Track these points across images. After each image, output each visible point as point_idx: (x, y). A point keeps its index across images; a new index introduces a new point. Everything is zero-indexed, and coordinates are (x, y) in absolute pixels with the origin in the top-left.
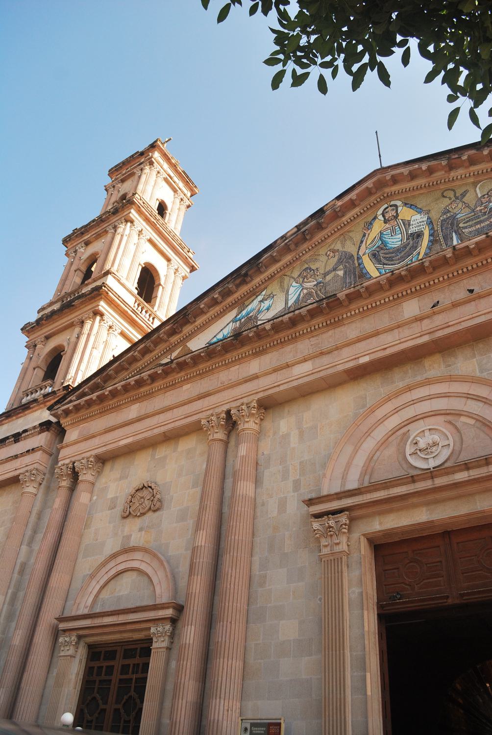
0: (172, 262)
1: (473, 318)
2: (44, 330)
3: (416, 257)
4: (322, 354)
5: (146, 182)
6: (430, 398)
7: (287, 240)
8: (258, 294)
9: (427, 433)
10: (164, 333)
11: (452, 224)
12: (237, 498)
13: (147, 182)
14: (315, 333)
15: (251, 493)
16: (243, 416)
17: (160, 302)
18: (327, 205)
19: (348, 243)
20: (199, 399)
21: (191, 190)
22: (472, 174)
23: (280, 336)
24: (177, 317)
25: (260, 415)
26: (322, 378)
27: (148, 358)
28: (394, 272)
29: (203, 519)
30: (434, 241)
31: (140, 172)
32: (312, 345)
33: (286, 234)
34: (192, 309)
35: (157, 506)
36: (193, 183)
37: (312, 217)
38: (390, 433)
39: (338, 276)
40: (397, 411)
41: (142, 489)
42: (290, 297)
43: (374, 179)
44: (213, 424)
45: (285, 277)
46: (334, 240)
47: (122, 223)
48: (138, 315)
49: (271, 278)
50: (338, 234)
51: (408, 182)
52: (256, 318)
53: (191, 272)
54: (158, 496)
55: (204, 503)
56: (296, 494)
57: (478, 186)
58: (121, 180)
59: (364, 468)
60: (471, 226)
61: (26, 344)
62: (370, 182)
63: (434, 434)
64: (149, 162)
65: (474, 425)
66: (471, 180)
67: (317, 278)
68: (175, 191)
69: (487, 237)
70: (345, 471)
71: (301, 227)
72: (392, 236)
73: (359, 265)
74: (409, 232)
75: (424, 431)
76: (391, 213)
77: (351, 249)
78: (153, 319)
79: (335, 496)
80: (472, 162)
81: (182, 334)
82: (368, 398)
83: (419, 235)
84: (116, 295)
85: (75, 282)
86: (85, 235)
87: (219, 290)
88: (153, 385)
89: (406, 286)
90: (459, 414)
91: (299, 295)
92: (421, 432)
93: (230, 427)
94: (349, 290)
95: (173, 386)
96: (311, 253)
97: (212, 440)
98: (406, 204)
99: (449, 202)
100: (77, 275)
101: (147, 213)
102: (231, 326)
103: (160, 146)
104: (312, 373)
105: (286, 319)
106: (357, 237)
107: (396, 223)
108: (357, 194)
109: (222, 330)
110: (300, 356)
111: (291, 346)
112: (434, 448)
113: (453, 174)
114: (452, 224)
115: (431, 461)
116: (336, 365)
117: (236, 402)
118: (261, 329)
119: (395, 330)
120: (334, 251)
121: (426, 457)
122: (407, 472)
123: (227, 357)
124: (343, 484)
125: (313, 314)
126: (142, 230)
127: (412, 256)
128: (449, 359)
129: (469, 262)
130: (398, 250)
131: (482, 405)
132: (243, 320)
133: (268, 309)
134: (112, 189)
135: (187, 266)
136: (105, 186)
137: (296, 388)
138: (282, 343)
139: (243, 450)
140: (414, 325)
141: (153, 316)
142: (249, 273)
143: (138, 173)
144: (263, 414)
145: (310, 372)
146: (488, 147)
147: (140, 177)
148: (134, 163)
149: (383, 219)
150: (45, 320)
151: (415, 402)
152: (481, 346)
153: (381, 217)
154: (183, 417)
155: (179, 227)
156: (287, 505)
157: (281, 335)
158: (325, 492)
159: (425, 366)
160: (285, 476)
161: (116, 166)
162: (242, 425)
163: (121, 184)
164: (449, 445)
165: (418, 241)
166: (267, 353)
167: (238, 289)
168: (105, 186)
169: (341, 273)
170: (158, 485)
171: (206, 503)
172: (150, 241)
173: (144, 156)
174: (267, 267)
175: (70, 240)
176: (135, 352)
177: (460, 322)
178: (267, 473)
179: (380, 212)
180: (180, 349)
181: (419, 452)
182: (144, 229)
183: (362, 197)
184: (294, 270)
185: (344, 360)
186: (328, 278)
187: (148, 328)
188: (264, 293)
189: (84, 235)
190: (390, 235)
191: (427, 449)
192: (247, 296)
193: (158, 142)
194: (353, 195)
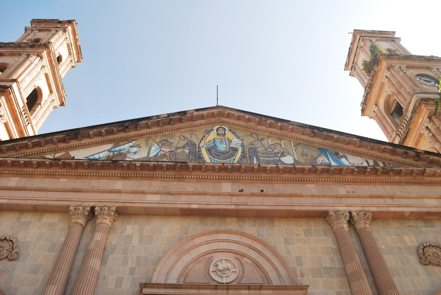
0: (53, 94)
1: (260, 205)
3: (233, 161)
4: (168, 193)
5: (57, 40)
6: (228, 241)
7: (160, 119)
8: (130, 141)
9: (224, 261)
10: (57, 138)
11: (254, 152)
12: (89, 269)
13: (58, 40)
14: (165, 180)
15: (98, 268)
16: (104, 214)
17: (36, 115)
18: (189, 111)
19: (194, 136)
20: (72, 191)
21: (79, 59)
22: (268, 131)
23: (143, 173)
24: (70, 132)
25: (115, 217)
26: (165, 208)
27: (36, 149)
28: (224, 164)
29: (57, 277)
30: (243, 156)
31: (55, 32)
32: (162, 186)
33: (160, 115)
34: (83, 132)
35: (14, 257)
36: (81, 55)
37: (179, 113)
38: (201, 255)
39: (185, 152)
40: (208, 243)
41: (3, 240)
43: (219, 110)
44: (79, 212)
45: (150, 139)
46: (186, 131)
47: (35, 55)
48: (22, 117)
49: (141, 136)
50: (188, 129)
51: (235, 120)
52: (125, 155)
53: (60, 105)
54: (17, 250)
55: (60, 265)
56: (131, 277)
57: (270, 138)
58: (39, 29)
59: (182, 272)
60: (264, 157)
62: (216, 110)
63: (227, 263)
64: (64, 30)
65: (251, 264)
66: (267, 134)
67: (172, 148)
68: (70, 54)
69: (277, 166)
70: (169, 270)
71: (170, 115)
73: (199, 151)
74: (231, 146)
75: (222, 259)
76: (221, 132)
77: (196, 141)
78: (28, 123)
79: (163, 286)
80: (271, 126)
81: (68, 144)
82: (190, 229)
83: (236, 150)
84: (15, 98)
86: (2, 49)
87: (107, 128)
88: (36, 170)
89: (228, 174)
90: (244, 256)
91: (158, 153)
92: (220, 260)
93: (90, 218)
94: (196, 163)
95: (53, 176)
96: (170, 132)
97: (76, 222)
98: (230, 131)
99: (254, 140)
102: (106, 154)
103: (74, 24)
104: (159, 203)
105: (152, 164)
106: (200, 136)
107: (223, 138)
108: (207, 113)
109: (98, 153)
110: (152, 189)
111: (148, 181)
112: (227, 272)
113: (259, 127)
114: (254, 152)
115: (224, 278)
116: (176, 203)
117: (100, 203)
118: (132, 164)
119: (216, 196)
121: (222, 275)
122: (209, 282)
123: (101, 172)
124: (166, 279)
125: (169, 168)
126: (45, 66)
128: (241, 223)
129: (264, 175)
130: (223, 153)
131: (257, 255)
132: (115, 153)
133: (135, 153)
134: (30, 31)
135: (60, 101)
136: (26, 27)
137: (146, 208)
138: (143, 178)
139: (98, 236)
140: (227, 197)
141: (29, 121)
142: (130, 127)
144: (116, 217)
145: (159, 202)
146: (281, 122)
147: (54, 35)
148: (52, 24)
149: (216, 132)
151: (219, 241)
152: (259, 221)
153: (215, 131)
154: (56, 199)
156: (123, 283)
157: (144, 172)
158: (154, 281)
159: (227, 222)
160: (125, 262)
162: (101, 219)
164: (236, 272)
165: (235, 153)
166: (130, 180)
168: (26, 27)
170: (18, 241)
171: (61, 266)
172: (46, 75)
173: (61, 24)
174: (142, 128)
177: (254, 205)
178: (111, 257)
180: (63, 153)
181: (217, 271)
182: (46, 66)
184: (157, 138)
185: (182, 202)
186: (179, 151)
187: (24, 128)
188: (134, 142)
191: (223, 271)
192: (122, 140)
193: (74, 22)
194: (205, 113)
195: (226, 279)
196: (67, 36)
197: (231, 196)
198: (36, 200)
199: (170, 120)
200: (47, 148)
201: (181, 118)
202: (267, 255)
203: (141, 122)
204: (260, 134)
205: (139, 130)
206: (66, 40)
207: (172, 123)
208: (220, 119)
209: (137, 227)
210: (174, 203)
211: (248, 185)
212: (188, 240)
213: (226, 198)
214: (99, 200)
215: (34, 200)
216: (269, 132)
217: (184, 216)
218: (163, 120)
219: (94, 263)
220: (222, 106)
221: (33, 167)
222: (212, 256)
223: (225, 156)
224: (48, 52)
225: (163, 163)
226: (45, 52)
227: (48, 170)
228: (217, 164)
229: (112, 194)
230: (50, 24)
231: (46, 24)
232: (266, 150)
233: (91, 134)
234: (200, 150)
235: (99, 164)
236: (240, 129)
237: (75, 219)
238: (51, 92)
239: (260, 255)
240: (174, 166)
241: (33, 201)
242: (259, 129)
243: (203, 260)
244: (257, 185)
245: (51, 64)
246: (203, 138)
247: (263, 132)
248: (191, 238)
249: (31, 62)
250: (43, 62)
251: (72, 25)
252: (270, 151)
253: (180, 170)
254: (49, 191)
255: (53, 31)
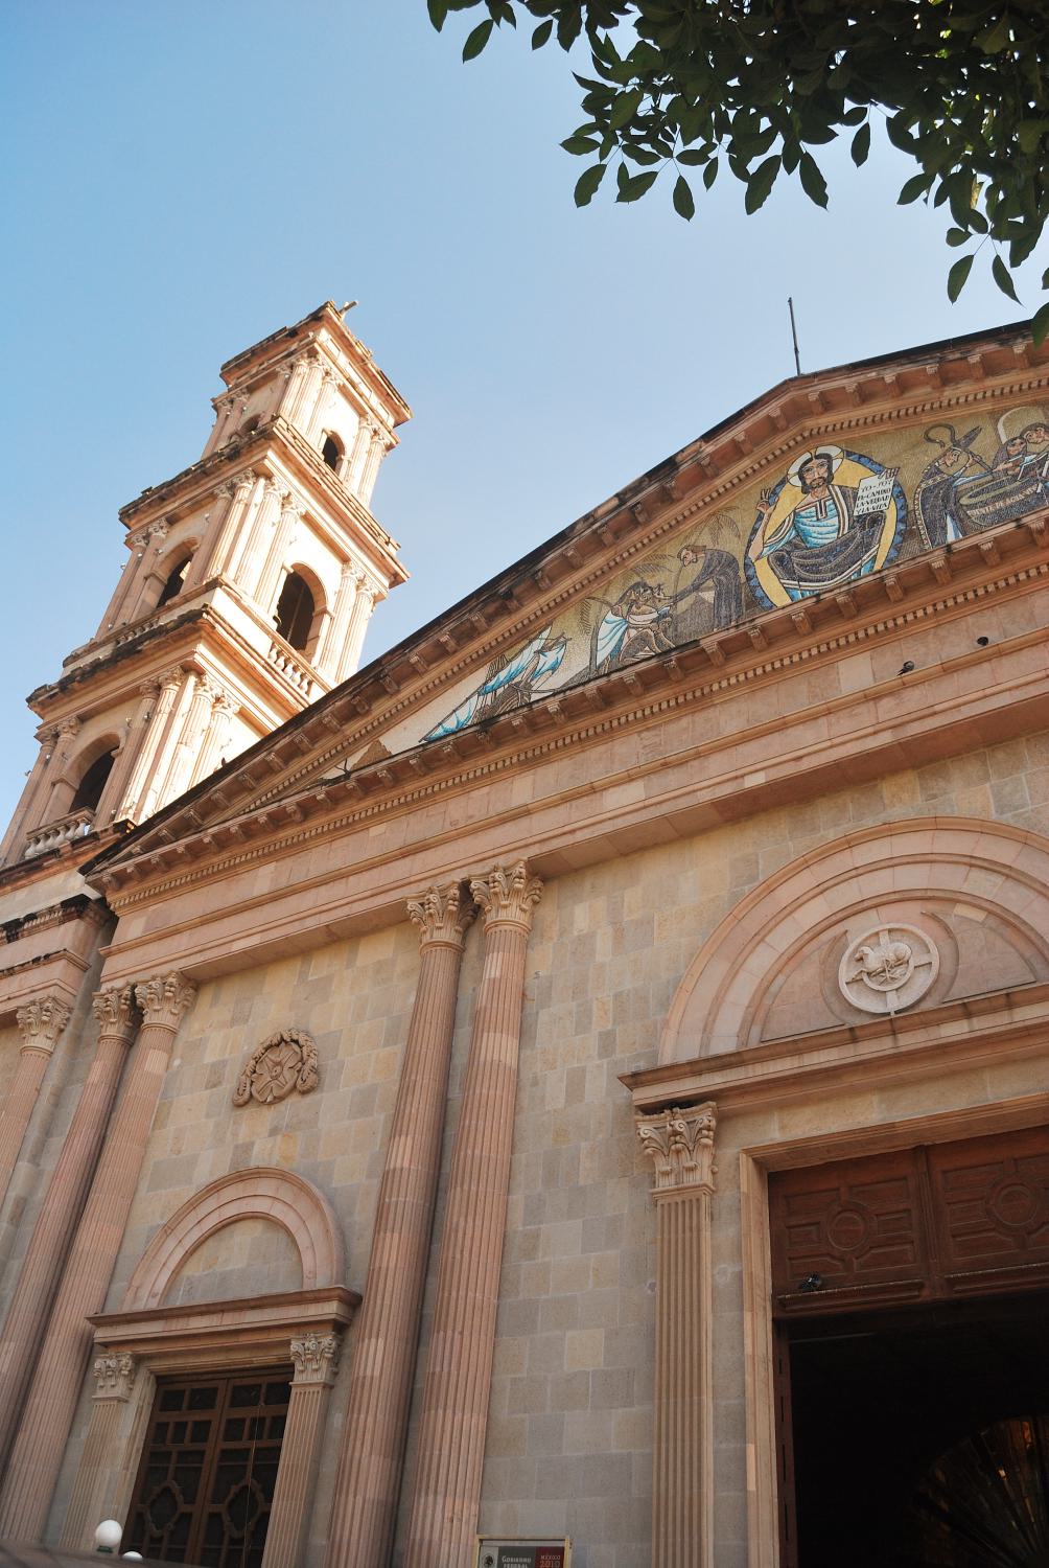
0: (352, 564)
1: (986, 697)
2: (76, 704)
3: (868, 566)
5: (301, 393)
6: (892, 863)
8: (533, 636)
9: (884, 938)
11: (946, 499)
14: (651, 723)
15: (510, 1058)
16: (496, 894)
17: (325, 648)
18: (682, 451)
19: (726, 532)
20: (404, 856)
21: (396, 412)
22: (989, 394)
26: (664, 817)
27: (296, 766)
28: (822, 597)
30: (906, 534)
31: (288, 371)
33: (596, 510)
35: (309, 1083)
36: (400, 398)
37: (651, 475)
38: (807, 937)
39: (703, 601)
40: (821, 889)
41: (278, 1045)
42: (601, 644)
46: (696, 525)
47: (247, 478)
48: (276, 676)
49: (562, 602)
50: (704, 514)
51: (855, 406)
52: (528, 687)
53: (392, 585)
54: (312, 1062)
55: (410, 1078)
56: (605, 1061)
57: (1003, 418)
60: (985, 504)
61: (37, 731)
63: (898, 941)
64: (308, 351)
65: (983, 924)
66: (988, 406)
67: (659, 605)
69: (1019, 527)
70: (709, 1014)
72: (818, 520)
73: (749, 579)
74: (856, 514)
75: (877, 934)
76: (817, 472)
77: (732, 545)
78: (310, 683)
79: (688, 1069)
80: (990, 368)
81: (370, 718)
82: (761, 861)
83: (875, 520)
85: (143, 601)
87: (452, 626)
88: (306, 825)
89: (849, 626)
90: (952, 899)
91: (621, 640)
92: (871, 936)
93: (469, 918)
95: (348, 827)
98: (849, 454)
99: (940, 451)
100: (149, 588)
101: (301, 460)
102: (475, 704)
103: (331, 318)
104: (645, 807)
106: (745, 521)
109: (454, 711)
111: (601, 748)
112: (899, 971)
113: (949, 393)
114: (946, 499)
116: (694, 791)
117: (480, 864)
120: (695, 550)
121: (881, 988)
124: (705, 1043)
125: (648, 681)
126: (290, 494)
127: (861, 564)
129: (981, 578)
130: (830, 551)
133: (553, 669)
134: (229, 406)
136: (213, 400)
138: (583, 742)
139: (494, 967)
141: (309, 677)
142: (516, 591)
143: (284, 373)
145: (641, 805)
146: (1024, 337)
147: (287, 382)
149: (800, 484)
150: (79, 682)
151: (860, 871)
152: (1000, 755)
153: (796, 481)
155: (369, 490)
156: (587, 1085)
157: (582, 724)
159: (881, 797)
160: (582, 1026)
161: (237, 358)
162: (493, 912)
163: (247, 396)
164: (930, 963)
165: (873, 534)
166: (549, 762)
167: (489, 626)
168: (213, 400)
169: (709, 596)
171: (413, 1078)
172: (307, 519)
175: (135, 512)
176: (269, 754)
178: (544, 1017)
179: (795, 468)
181: (866, 978)
183: (757, 437)
185: (712, 780)
186: (683, 606)
188: (545, 634)
189: (165, 503)
190: (815, 519)
191: (884, 971)
193: (328, 309)
194: (738, 432)
195: (899, 998)
196: (326, 367)
197: (874, 699)
198: (324, 911)
199: (633, 513)
200: (320, 751)
201: (663, 489)
202: (1035, 874)
203: (548, 559)
204: (964, 419)
205: (547, 590)
206: (328, 379)
207: (641, 519)
208: (804, 429)
209: (601, 904)
210: (688, 793)
211: (931, 637)
212: (755, 898)
213: (855, 715)
214: (476, 858)
215: (320, 912)
216: (993, 395)
217: (739, 822)
218: (610, 523)
219: (499, 1047)
220: (785, 382)
221: (555, 723)
222: (843, 930)
223: (840, 559)
224: (280, 450)
225: (625, 671)
226: (270, 453)
227: (332, 815)
228: (795, 606)
229: (507, 826)
230: (271, 354)
231: (260, 361)
232: (990, 471)
233: (416, 663)
234: (750, 572)
235: (448, 749)
236: (884, 433)
237: (428, 934)
238: (345, 560)
239: (1010, 884)
240: (660, 667)
241: (297, 923)
242: (950, 401)
243: (814, 951)
244: (963, 623)
245: (307, 478)
246: (757, 526)
247: (970, 405)
248: (764, 890)
249: (246, 505)
250: (276, 487)
251: (328, 322)
252: (1007, 470)
253: (686, 676)
254: (348, 876)
255: (282, 372)
